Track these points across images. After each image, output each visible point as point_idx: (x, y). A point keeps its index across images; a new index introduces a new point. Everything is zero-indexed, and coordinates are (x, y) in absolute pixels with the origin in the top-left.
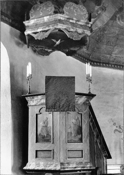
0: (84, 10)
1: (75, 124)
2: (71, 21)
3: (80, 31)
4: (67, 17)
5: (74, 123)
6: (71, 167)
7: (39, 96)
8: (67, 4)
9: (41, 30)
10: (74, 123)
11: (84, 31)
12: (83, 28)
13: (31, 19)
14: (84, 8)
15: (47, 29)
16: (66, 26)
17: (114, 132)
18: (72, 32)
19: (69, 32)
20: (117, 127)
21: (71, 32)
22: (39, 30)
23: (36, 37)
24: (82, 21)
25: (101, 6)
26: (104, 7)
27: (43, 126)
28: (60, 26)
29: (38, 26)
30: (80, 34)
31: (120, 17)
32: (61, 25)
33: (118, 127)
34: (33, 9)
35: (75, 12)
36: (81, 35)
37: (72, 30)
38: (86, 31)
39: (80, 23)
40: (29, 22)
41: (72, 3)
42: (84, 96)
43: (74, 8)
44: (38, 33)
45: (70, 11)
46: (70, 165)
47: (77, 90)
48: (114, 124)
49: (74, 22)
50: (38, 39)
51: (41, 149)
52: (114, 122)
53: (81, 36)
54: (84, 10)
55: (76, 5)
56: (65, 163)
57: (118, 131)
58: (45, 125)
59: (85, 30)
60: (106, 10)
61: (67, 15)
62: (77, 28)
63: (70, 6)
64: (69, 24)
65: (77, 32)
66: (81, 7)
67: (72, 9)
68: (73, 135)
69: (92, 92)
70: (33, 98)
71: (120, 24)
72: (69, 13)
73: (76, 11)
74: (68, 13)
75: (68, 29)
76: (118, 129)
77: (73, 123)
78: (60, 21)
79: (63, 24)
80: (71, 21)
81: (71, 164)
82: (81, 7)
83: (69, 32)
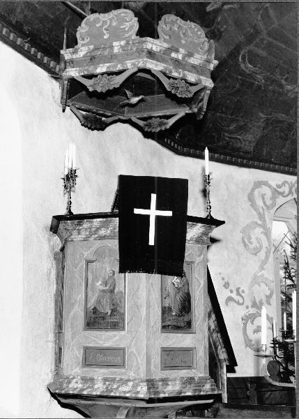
0: (201, 34)
1: (178, 289)
2: (173, 55)
3: (192, 78)
4: (166, 45)
5: (176, 286)
6: (171, 389)
7: (95, 220)
8: (165, 20)
9: (104, 70)
10: (176, 286)
11: (200, 80)
12: (198, 72)
13: (79, 45)
14: (199, 30)
15: (119, 67)
16: (163, 65)
17: (227, 304)
18: (176, 79)
19: (169, 78)
20: (231, 292)
21: (174, 78)
22: (101, 69)
23: (91, 86)
24: (197, 56)
25: (213, 28)
26: (218, 30)
27: (103, 291)
28: (155, 66)
29: (97, 60)
30: (192, 84)
31: (247, 55)
32: (152, 63)
33: (235, 292)
34: (86, 24)
35: (182, 35)
36: (193, 87)
37: (175, 74)
38: (204, 78)
39: (193, 61)
40: (73, 53)
41: (176, 18)
42: (200, 225)
43: (179, 27)
44: (96, 76)
45: (173, 36)
46: (168, 385)
47: (190, 213)
48: (224, 286)
49: (180, 57)
50: (97, 90)
51: (97, 344)
52: (226, 280)
53: (194, 89)
54: (199, 33)
55: (183, 22)
56: (157, 379)
57: (235, 301)
58: (108, 287)
59: (201, 77)
60: (220, 36)
61: (165, 40)
62: (186, 72)
63: (173, 23)
64: (170, 61)
65: (186, 80)
66: (193, 27)
67: (176, 29)
68: (174, 314)
69: (216, 216)
70: (79, 224)
71: (244, 69)
72: (170, 38)
73: (184, 34)
74: (167, 37)
75: (167, 72)
76: (234, 295)
77: (174, 284)
78: (151, 54)
79: (158, 61)
80: (173, 55)
81: (170, 383)
82: (193, 27)
83: (169, 78)
